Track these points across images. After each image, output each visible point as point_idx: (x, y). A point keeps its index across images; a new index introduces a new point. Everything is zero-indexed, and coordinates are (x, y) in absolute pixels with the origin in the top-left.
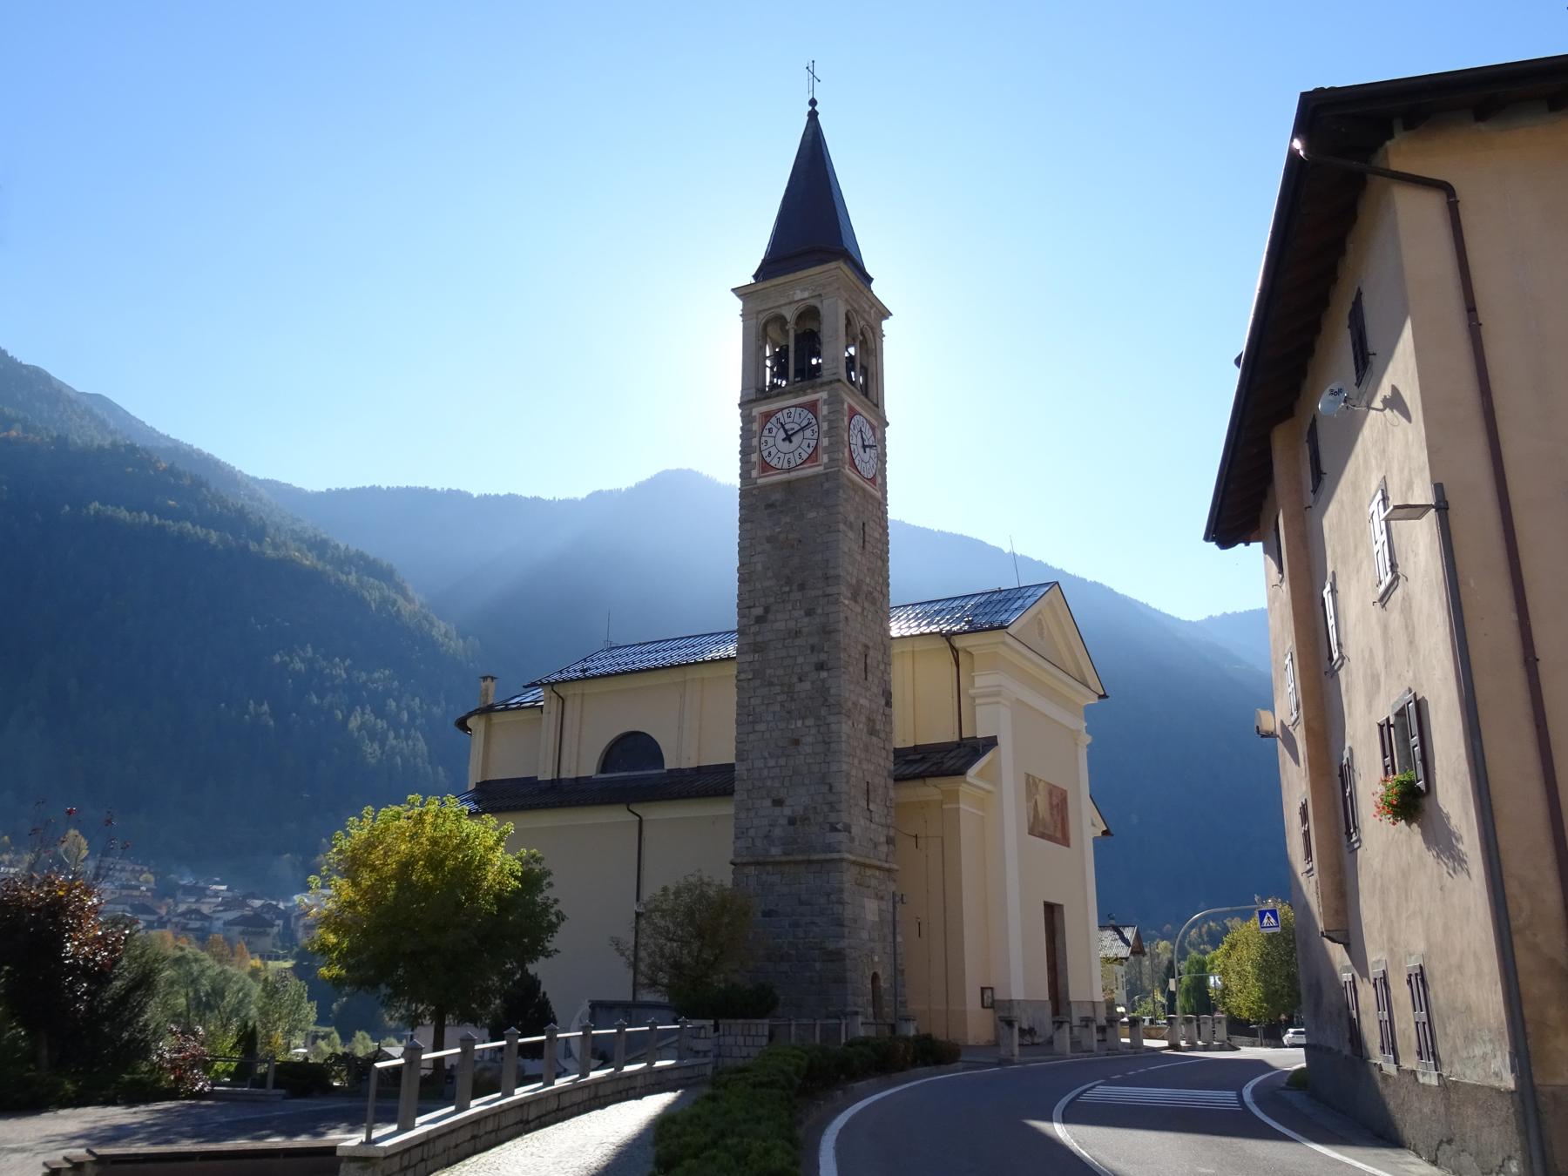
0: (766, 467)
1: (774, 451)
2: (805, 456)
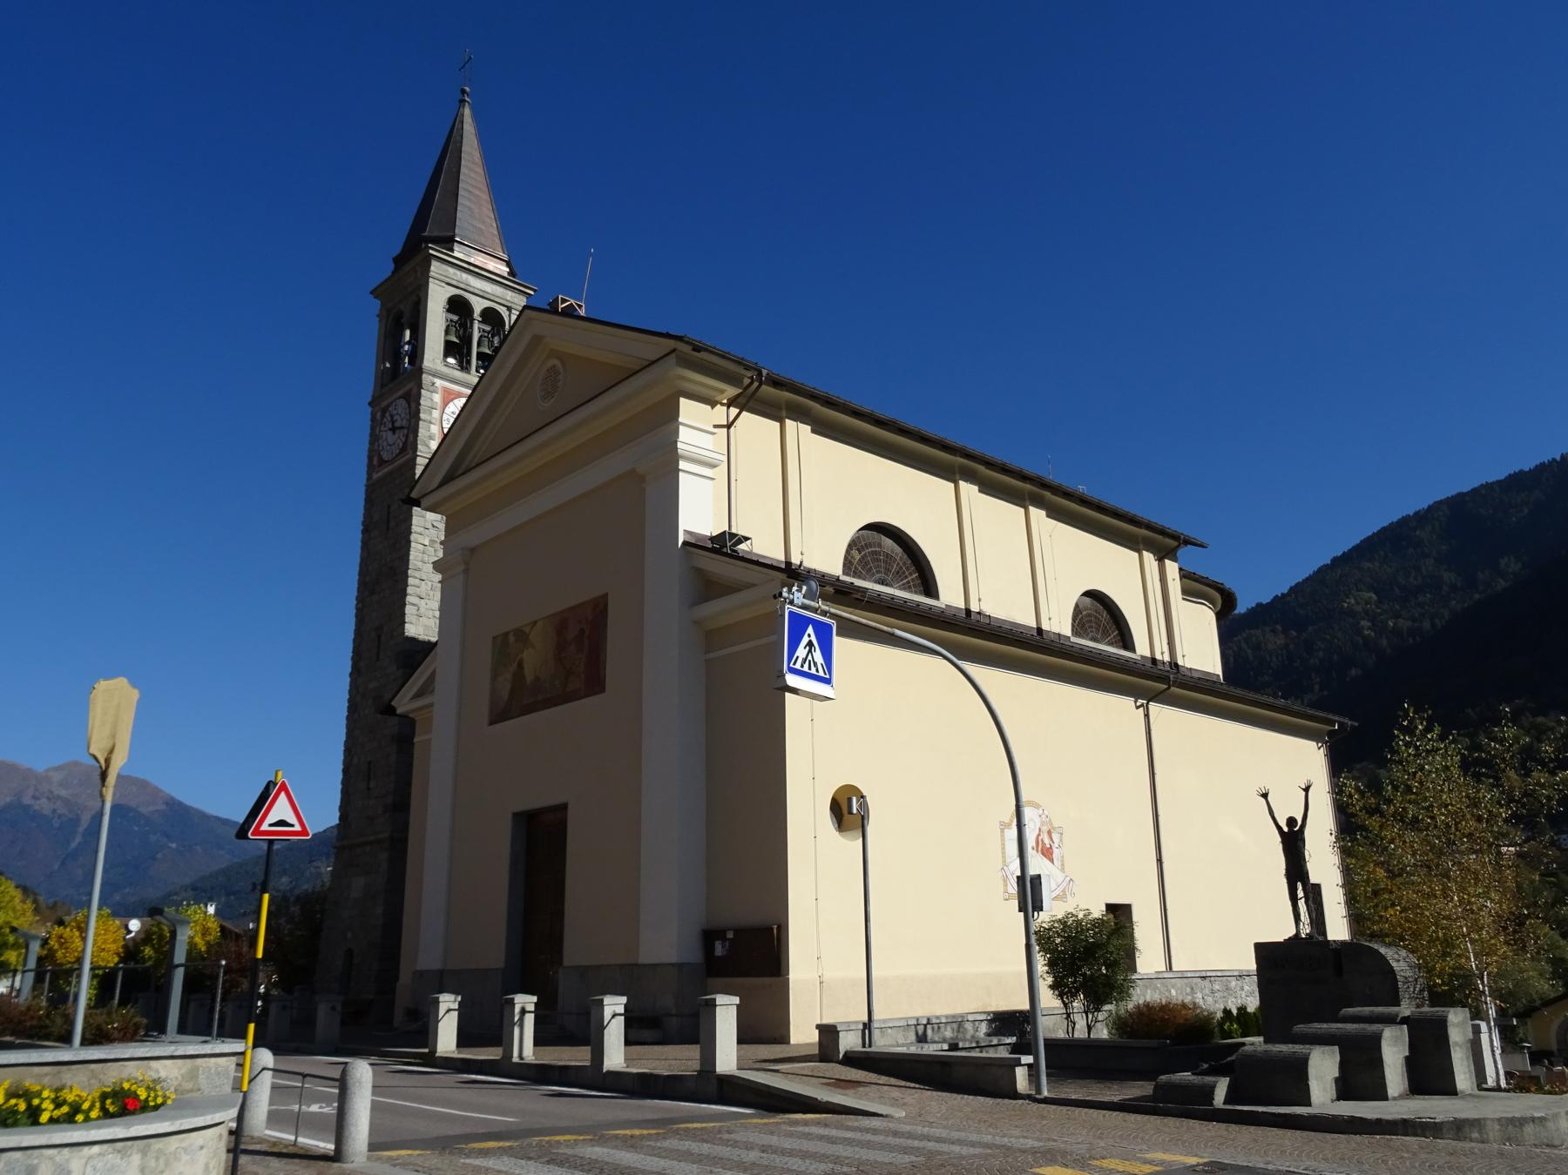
0: (382, 462)
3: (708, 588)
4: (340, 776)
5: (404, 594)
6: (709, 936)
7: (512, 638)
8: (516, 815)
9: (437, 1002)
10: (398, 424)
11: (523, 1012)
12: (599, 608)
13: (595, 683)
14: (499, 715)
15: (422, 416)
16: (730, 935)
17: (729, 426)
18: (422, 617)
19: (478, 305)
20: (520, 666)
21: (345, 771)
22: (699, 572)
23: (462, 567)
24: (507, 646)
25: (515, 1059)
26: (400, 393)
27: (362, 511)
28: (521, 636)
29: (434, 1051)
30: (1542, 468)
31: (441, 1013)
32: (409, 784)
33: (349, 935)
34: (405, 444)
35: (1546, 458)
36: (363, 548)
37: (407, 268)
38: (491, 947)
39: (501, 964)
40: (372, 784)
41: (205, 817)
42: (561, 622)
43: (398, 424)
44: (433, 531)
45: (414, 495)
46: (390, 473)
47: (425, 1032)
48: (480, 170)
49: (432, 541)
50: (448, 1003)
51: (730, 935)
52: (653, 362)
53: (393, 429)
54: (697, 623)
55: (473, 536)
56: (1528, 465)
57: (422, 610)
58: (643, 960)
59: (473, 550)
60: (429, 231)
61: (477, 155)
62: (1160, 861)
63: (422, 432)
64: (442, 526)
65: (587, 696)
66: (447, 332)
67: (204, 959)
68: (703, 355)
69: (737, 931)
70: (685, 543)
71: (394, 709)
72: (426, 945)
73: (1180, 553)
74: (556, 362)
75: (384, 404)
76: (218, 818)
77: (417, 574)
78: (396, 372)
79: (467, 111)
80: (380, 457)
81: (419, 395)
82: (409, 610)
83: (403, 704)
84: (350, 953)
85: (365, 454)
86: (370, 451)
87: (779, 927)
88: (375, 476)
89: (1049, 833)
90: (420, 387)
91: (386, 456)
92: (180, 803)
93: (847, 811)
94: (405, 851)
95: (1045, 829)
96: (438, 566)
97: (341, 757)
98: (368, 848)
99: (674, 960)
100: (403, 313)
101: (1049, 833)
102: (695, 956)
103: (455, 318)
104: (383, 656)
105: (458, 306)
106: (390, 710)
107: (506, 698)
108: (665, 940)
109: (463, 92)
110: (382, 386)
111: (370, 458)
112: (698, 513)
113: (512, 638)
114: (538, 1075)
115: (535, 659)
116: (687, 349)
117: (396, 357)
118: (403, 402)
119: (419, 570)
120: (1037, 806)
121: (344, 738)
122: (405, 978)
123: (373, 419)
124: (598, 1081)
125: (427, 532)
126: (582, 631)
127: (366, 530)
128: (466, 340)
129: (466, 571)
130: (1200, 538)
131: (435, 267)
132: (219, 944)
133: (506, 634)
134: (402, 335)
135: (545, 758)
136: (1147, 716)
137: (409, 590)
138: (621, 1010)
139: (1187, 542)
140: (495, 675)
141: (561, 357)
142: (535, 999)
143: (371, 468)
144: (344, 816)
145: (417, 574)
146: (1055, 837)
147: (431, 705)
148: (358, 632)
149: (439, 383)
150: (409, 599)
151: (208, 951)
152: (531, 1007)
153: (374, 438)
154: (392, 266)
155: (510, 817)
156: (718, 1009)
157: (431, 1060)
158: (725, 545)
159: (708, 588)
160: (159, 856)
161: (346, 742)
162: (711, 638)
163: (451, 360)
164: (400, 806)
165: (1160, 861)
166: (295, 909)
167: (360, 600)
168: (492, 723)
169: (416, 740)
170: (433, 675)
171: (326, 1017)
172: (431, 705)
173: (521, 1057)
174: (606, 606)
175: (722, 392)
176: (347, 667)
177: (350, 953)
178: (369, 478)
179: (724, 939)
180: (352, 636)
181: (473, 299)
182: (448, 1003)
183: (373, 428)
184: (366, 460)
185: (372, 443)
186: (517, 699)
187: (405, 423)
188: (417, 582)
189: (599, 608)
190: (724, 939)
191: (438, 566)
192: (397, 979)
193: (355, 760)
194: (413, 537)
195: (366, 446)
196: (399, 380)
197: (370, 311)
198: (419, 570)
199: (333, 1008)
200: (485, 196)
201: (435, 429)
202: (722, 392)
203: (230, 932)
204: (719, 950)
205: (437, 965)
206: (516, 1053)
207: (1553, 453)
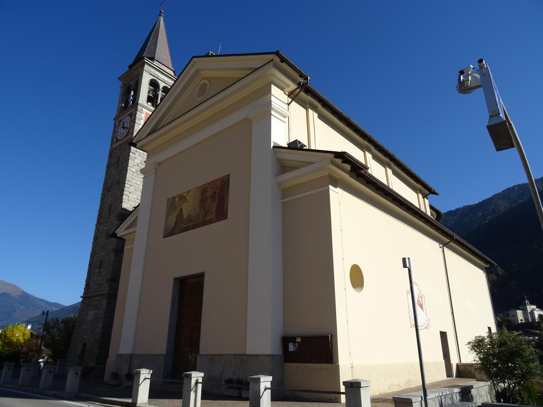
0: (117, 140)
3: (283, 167)
5: (123, 190)
6: (286, 340)
7: (177, 199)
8: (176, 279)
9: (139, 374)
10: (125, 126)
11: (197, 383)
12: (224, 184)
14: (169, 233)
18: (131, 199)
19: (162, 85)
20: (181, 211)
21: (90, 265)
22: (279, 161)
23: (154, 171)
24: (173, 204)
26: (128, 113)
27: (107, 160)
28: (182, 198)
30: (457, 210)
31: (141, 379)
33: (85, 336)
34: (128, 133)
35: (458, 207)
36: (106, 174)
37: (134, 68)
38: (159, 343)
39: (164, 352)
40: (102, 270)
41: (34, 298)
42: (203, 190)
43: (125, 126)
44: (137, 167)
45: (134, 141)
46: (121, 144)
48: (166, 39)
50: (145, 374)
51: (299, 340)
52: (258, 68)
53: (124, 128)
54: (279, 184)
55: (160, 157)
56: (453, 209)
57: (130, 198)
58: (248, 352)
59: (159, 164)
60: (143, 56)
61: (165, 34)
62: (453, 313)
63: (138, 116)
64: (146, 157)
66: (149, 92)
67: (22, 346)
68: (284, 65)
69: (303, 338)
70: (274, 147)
71: (116, 234)
75: (120, 119)
76: (38, 299)
77: (129, 183)
78: (126, 107)
79: (162, 18)
81: (136, 113)
82: (124, 197)
83: (120, 232)
84: (85, 345)
85: (110, 144)
86: (112, 137)
87: (331, 336)
88: (114, 146)
89: (421, 297)
90: (136, 110)
91: (119, 138)
92: (26, 293)
93: (357, 278)
94: (115, 299)
95: (420, 295)
96: (142, 171)
98: (97, 298)
99: (269, 353)
100: (131, 85)
101: (421, 297)
103: (152, 88)
104: (111, 213)
105: (154, 84)
106: (114, 235)
107: (173, 225)
108: (263, 341)
109: (161, 12)
110: (120, 112)
111: (112, 139)
112: (280, 136)
113: (177, 199)
115: (189, 208)
116: (277, 59)
117: (127, 102)
118: (129, 117)
119: (130, 181)
120: (417, 285)
121: (91, 251)
123: (115, 125)
125: (137, 159)
126: (215, 193)
127: (108, 167)
128: (156, 96)
129: (156, 172)
130: (437, 191)
131: (146, 67)
132: (29, 340)
133: (174, 197)
134: (130, 93)
135: (193, 252)
136: (443, 251)
137: (125, 189)
140: (167, 216)
141: (207, 78)
142: (202, 374)
143: (112, 143)
144: (86, 297)
145: (129, 183)
146: (423, 299)
147: (135, 232)
149: (144, 110)
150: (125, 192)
151: (24, 343)
152: (200, 380)
153: (115, 131)
154: (128, 69)
156: (361, 389)
158: (295, 146)
159: (283, 167)
160: (17, 310)
161: (91, 253)
162: (285, 192)
163: (149, 104)
164: (114, 279)
166: (62, 326)
168: (164, 237)
169: (125, 248)
170: (137, 217)
171: (72, 379)
172: (135, 232)
174: (228, 180)
176: (95, 222)
177: (85, 345)
178: (111, 146)
180: (98, 209)
182: (145, 374)
183: (114, 128)
184: (110, 140)
185: (113, 134)
188: (129, 186)
189: (224, 184)
191: (142, 171)
192: (107, 357)
193: (95, 261)
194: (129, 168)
195: (111, 135)
196: (129, 106)
197: (116, 90)
198: (130, 181)
200: (167, 48)
201: (143, 116)
202: (289, 86)
203: (34, 335)
205: (129, 352)
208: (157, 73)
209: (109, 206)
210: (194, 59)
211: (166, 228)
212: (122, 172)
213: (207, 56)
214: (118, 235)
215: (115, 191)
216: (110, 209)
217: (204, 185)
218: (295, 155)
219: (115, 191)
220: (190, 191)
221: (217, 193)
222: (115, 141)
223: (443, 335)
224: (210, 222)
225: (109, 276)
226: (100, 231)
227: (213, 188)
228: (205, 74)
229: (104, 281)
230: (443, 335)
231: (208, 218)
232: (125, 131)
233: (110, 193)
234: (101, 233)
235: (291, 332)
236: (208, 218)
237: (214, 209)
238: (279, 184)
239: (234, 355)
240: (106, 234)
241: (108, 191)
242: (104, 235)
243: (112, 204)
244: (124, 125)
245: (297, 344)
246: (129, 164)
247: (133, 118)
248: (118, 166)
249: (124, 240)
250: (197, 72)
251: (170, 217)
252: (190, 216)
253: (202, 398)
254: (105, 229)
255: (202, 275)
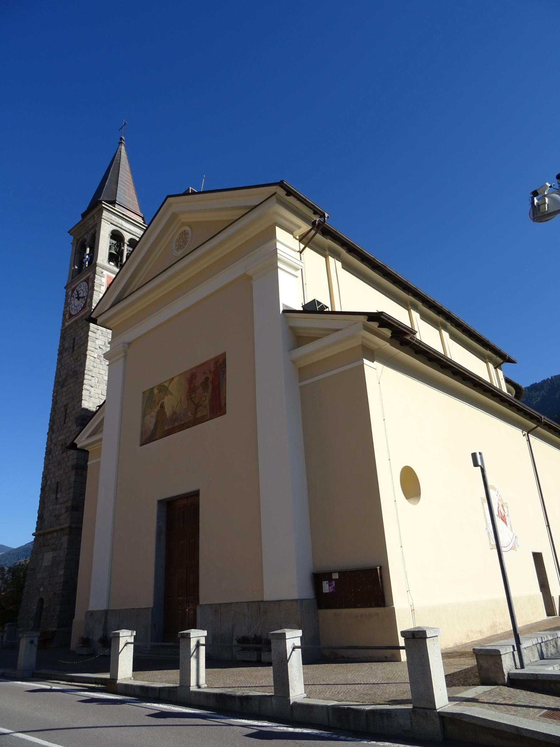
0: (71, 316)
1: (73, 307)
2: (82, 305)
3: (299, 338)
4: (39, 492)
6: (318, 578)
7: (156, 391)
8: (160, 502)
9: (118, 637)
10: (81, 295)
11: (198, 645)
12: (224, 355)
13: (218, 408)
14: (148, 438)
15: (95, 288)
16: (336, 576)
17: (301, 252)
19: (127, 237)
20: (162, 407)
21: (42, 489)
22: (292, 329)
23: (123, 354)
24: (150, 398)
25: (193, 687)
28: (163, 389)
29: (114, 679)
30: (544, 382)
31: (121, 645)
32: (83, 494)
33: (42, 589)
34: (85, 305)
38: (143, 592)
40: (59, 495)
42: (191, 377)
43: (81, 295)
44: (99, 350)
45: (93, 316)
46: (76, 321)
47: (108, 662)
49: (98, 355)
50: (126, 636)
51: (336, 576)
53: (78, 298)
54: (294, 362)
57: (92, 393)
59: (129, 344)
61: (128, 168)
62: (548, 526)
65: (211, 418)
66: (110, 248)
68: (291, 199)
69: (342, 573)
70: (284, 311)
72: (96, 592)
73: (502, 366)
74: (187, 228)
77: (90, 373)
79: (123, 148)
80: (70, 314)
82: (84, 392)
83: (81, 442)
84: (41, 601)
88: (67, 324)
89: (502, 506)
90: (95, 273)
91: (73, 313)
93: (410, 484)
95: (500, 504)
97: (40, 481)
98: (55, 534)
99: (296, 596)
101: (502, 506)
102: (308, 593)
103: (115, 242)
104: (68, 418)
105: (116, 236)
106: (73, 446)
107: (152, 427)
108: (285, 579)
109: (121, 139)
110: (72, 278)
111: (64, 315)
112: (291, 295)
113: (156, 391)
114: (223, 706)
115: (172, 403)
116: (282, 192)
117: (81, 263)
119: (90, 371)
120: (495, 489)
122: (79, 616)
123: (67, 295)
124: (277, 708)
125: (99, 339)
126: (207, 379)
128: (121, 253)
129: (125, 357)
131: (105, 214)
133: (152, 389)
134: (85, 251)
135: (187, 461)
136: (529, 440)
137: (85, 382)
138: (298, 643)
139: (510, 361)
140: (144, 416)
143: (64, 320)
147: (101, 440)
148: (54, 410)
149: (105, 272)
150: (85, 386)
152: (203, 641)
155: (156, 503)
157: (111, 685)
158: (313, 308)
159: (299, 338)
162: (302, 372)
163: (111, 263)
165: (548, 526)
167: (56, 391)
168: (142, 445)
169: (88, 463)
172: (101, 440)
173: (199, 686)
174: (225, 361)
175: (299, 227)
177: (41, 601)
178: (63, 324)
179: (330, 579)
181: (125, 234)
182: (126, 636)
183: (66, 300)
186: (160, 426)
187: (85, 295)
188: (90, 377)
190: (330, 579)
192: (73, 617)
193: (49, 483)
194: (88, 353)
196: (84, 268)
197: (67, 246)
198: (90, 371)
199: (32, 642)
202: (299, 227)
204: (326, 588)
205: (103, 607)
206: (193, 682)
207: (556, 374)
208: (121, 221)
209: (65, 406)
210: (170, 199)
211: (143, 433)
212: (79, 358)
213: (186, 193)
214: (78, 446)
215: (72, 385)
216: (66, 410)
217: (191, 370)
218: (313, 321)
219: (72, 385)
220: (172, 379)
221: (210, 379)
222: (67, 316)
223: (538, 558)
224: (203, 420)
225: (70, 504)
226: (54, 441)
227: (205, 373)
228: (185, 218)
229: (63, 511)
230: (538, 558)
231: (199, 415)
232: (81, 303)
233: (65, 389)
234: (55, 444)
235: (325, 566)
236: (199, 415)
237: (207, 402)
238: (294, 362)
239: (248, 603)
240: (62, 445)
241: (63, 386)
242: (59, 447)
243: (68, 404)
244: (78, 294)
245: (334, 583)
246: (89, 348)
247: (90, 284)
248: (73, 350)
249: (87, 451)
250: (174, 216)
251: (148, 417)
252: (174, 413)
253: (307, 660)
254: (60, 439)
255: (196, 494)
